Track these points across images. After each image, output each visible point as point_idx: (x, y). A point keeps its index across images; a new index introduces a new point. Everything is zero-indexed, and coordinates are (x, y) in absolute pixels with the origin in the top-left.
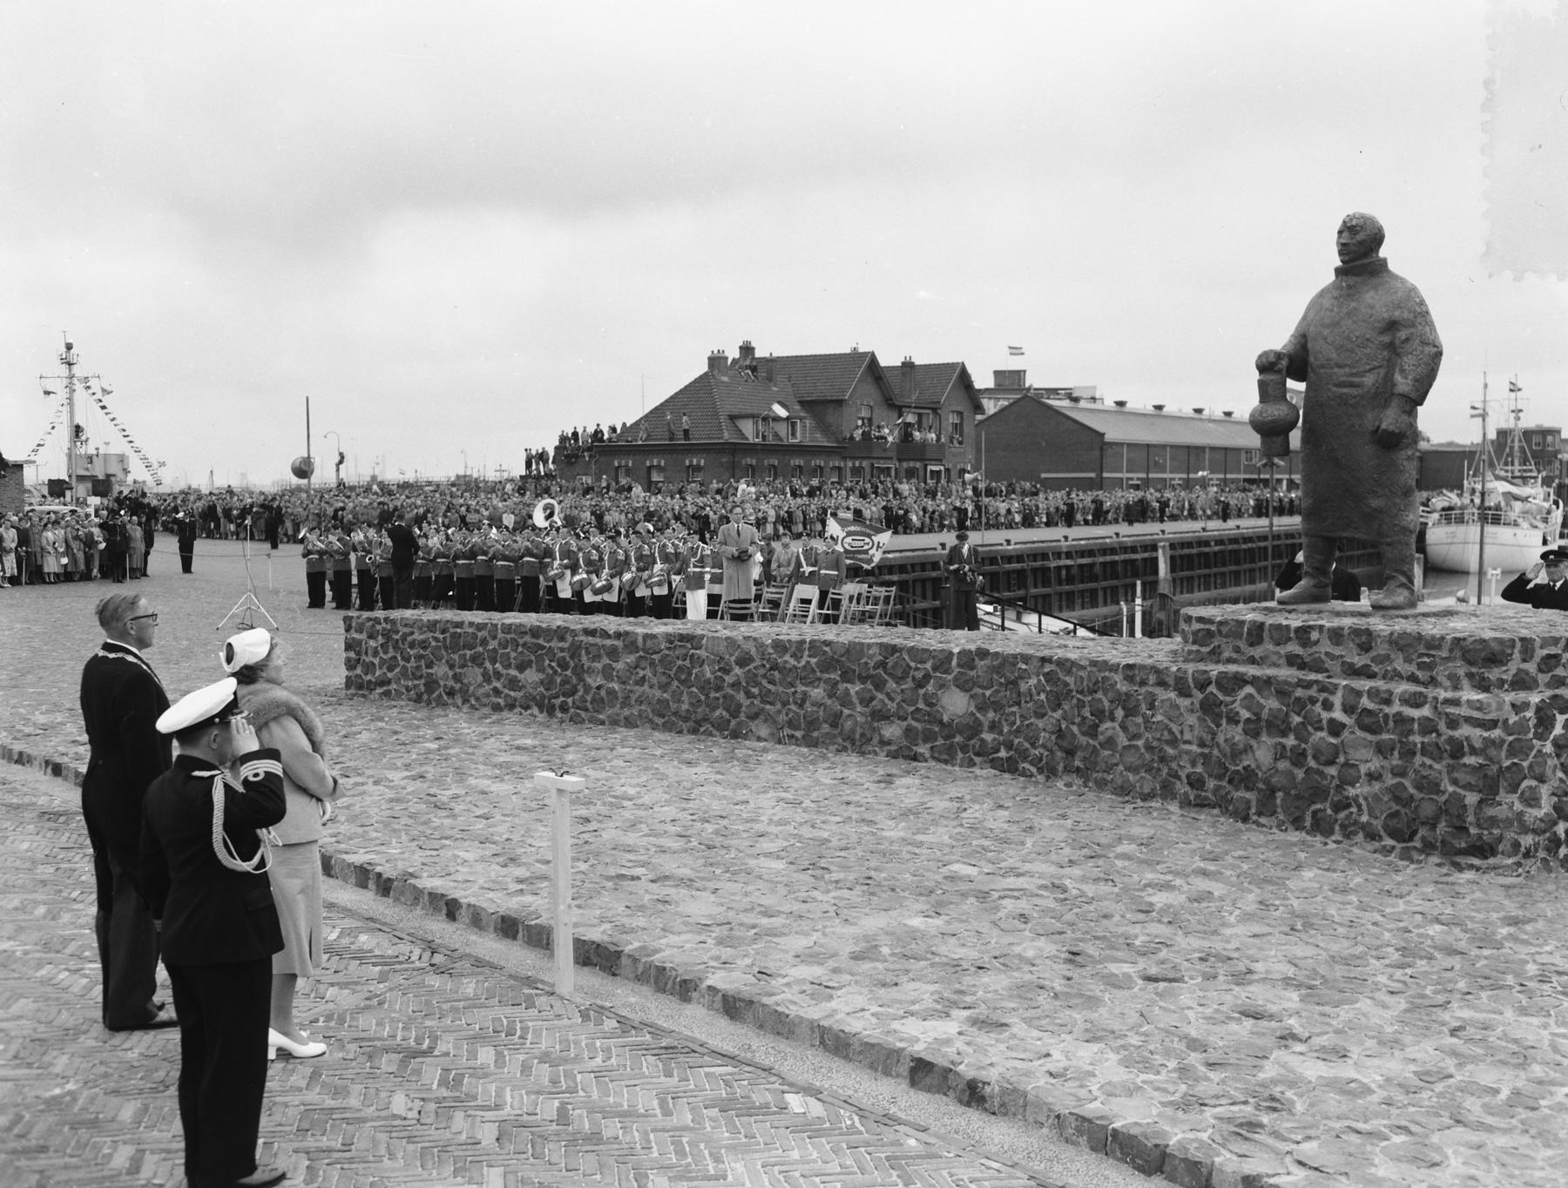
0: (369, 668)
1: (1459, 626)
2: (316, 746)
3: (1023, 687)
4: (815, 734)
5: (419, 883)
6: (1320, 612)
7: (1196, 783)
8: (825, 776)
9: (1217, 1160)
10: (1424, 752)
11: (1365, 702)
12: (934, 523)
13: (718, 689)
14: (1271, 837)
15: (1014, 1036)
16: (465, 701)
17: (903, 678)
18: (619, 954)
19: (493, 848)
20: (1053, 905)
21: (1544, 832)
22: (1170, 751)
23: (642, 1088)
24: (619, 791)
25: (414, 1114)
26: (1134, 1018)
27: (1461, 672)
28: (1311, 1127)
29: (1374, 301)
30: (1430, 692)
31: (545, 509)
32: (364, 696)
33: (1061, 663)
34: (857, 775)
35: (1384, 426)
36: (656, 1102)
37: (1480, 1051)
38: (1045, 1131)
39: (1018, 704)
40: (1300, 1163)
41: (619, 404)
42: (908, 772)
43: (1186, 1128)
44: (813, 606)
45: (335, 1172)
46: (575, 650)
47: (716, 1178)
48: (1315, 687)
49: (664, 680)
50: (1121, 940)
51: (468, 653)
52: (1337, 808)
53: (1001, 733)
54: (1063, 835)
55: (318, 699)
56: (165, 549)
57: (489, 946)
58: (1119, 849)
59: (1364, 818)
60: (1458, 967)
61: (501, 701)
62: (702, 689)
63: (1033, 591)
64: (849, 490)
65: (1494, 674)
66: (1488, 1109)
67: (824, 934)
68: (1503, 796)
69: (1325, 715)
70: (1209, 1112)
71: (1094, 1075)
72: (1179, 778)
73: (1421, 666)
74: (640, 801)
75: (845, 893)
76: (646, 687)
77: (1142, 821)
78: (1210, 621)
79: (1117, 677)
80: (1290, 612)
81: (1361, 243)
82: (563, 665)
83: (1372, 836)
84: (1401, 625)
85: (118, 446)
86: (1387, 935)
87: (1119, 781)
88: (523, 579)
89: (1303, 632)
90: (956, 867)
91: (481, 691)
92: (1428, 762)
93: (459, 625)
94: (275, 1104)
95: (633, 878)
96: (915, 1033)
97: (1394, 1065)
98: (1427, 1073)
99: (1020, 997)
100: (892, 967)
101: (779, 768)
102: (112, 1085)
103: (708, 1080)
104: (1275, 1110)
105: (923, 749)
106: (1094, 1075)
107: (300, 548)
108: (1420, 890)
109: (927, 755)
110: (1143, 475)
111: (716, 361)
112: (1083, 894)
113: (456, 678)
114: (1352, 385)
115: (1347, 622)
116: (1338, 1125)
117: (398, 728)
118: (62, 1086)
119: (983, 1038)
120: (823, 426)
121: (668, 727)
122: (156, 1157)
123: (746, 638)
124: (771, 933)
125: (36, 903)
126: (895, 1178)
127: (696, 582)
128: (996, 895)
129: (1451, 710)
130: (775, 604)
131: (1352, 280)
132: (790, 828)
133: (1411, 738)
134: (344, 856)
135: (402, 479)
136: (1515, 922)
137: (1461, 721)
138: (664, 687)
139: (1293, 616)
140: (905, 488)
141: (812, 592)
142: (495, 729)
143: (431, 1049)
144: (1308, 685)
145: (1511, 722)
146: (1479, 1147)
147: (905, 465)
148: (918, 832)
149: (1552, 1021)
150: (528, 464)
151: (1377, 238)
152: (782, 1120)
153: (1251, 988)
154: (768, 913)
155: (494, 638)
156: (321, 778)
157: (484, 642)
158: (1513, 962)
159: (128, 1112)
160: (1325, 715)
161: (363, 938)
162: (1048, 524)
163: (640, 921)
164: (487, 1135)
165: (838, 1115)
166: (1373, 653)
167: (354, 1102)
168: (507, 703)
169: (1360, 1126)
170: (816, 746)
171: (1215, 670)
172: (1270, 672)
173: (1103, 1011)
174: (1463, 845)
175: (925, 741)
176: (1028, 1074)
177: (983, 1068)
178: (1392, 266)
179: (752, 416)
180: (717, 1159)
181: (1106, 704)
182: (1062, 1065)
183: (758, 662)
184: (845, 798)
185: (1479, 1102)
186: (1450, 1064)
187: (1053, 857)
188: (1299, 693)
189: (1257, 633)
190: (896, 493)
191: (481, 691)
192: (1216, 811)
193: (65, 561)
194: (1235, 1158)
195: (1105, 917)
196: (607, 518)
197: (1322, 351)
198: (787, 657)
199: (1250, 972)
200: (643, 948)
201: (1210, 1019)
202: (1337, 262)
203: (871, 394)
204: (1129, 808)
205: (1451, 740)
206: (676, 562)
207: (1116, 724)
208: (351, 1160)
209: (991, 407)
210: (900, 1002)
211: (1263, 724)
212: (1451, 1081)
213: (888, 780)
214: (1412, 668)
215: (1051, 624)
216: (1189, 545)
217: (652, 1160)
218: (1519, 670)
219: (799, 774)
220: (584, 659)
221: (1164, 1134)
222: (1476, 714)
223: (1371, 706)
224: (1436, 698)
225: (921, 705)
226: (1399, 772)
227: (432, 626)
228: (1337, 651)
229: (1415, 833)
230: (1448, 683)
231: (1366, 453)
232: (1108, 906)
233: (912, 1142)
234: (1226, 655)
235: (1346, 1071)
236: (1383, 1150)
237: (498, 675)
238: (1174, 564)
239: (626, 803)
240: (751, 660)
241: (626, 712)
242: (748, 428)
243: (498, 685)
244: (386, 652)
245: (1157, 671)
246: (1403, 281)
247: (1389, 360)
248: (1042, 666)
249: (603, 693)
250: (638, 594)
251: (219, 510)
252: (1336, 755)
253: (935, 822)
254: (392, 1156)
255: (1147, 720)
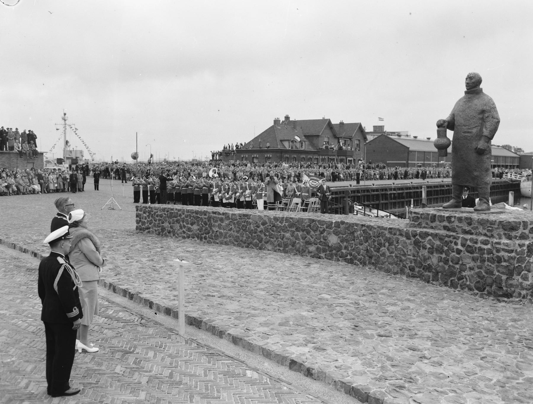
0: (144, 223)
1: (503, 217)
2: (97, 249)
3: (356, 234)
4: (287, 249)
5: (142, 296)
6: (457, 211)
7: (412, 269)
8: (287, 263)
9: (385, 398)
10: (488, 260)
11: (469, 243)
12: (349, 177)
13: (255, 233)
14: (436, 289)
15: (327, 354)
16: (174, 235)
17: (316, 231)
18: (201, 321)
19: (169, 285)
20: (353, 309)
21: (530, 289)
22: (403, 258)
23: (199, 366)
24: (216, 266)
25: (122, 373)
26: (370, 349)
27: (502, 233)
28: (421, 389)
29: (477, 103)
30: (491, 240)
31: (213, 171)
32: (142, 233)
33: (368, 227)
34: (298, 262)
35: (479, 147)
36: (203, 372)
37: (489, 365)
38: (331, 386)
39: (354, 240)
40: (414, 401)
41: (244, 135)
42: (316, 263)
43: (377, 387)
44: (299, 206)
45: (91, 391)
46: (209, 219)
47: (216, 398)
48: (452, 237)
49: (238, 229)
50: (374, 322)
51: (175, 219)
52: (459, 279)
53: (348, 250)
54: (363, 285)
55: (127, 233)
56: (90, 181)
57: (161, 318)
58: (381, 291)
59: (468, 283)
60: (490, 336)
61: (185, 235)
62: (250, 233)
63: (382, 202)
64: (320, 166)
65: (513, 234)
66: (486, 386)
67: (272, 317)
68: (515, 277)
69: (455, 247)
70: (388, 382)
71: (351, 368)
72: (406, 267)
73: (488, 231)
74: (222, 270)
75: (283, 303)
76: (232, 232)
77: (392, 282)
78: (418, 214)
79: (386, 232)
80: (446, 211)
81: (473, 83)
82: (206, 224)
83: (470, 289)
84: (484, 217)
85: (80, 147)
86: (468, 324)
87: (386, 268)
88: (203, 194)
89: (449, 218)
90: (323, 295)
91: (179, 232)
92: (490, 264)
93: (172, 209)
94: (78, 367)
95: (213, 296)
96: (293, 351)
97: (458, 369)
98: (468, 372)
99: (333, 340)
100: (292, 328)
101: (272, 260)
102: (27, 359)
103: (221, 365)
104: (411, 382)
105: (322, 255)
106: (351, 368)
107: (132, 183)
108: (484, 309)
109: (324, 257)
110: (423, 162)
111: (276, 122)
112: (365, 306)
113: (171, 227)
114: (468, 132)
115: (464, 215)
116: (431, 389)
117: (149, 244)
118: (11, 359)
119: (316, 354)
120: (312, 144)
121: (239, 245)
122: (34, 384)
123: (265, 216)
124: (254, 316)
125: (18, 298)
126: (276, 400)
127: (260, 197)
128: (335, 305)
129: (497, 246)
130: (286, 204)
131: (470, 96)
132: (270, 281)
133: (484, 256)
134: (120, 286)
135: (174, 160)
136: (515, 320)
137: (501, 250)
138: (238, 232)
139: (447, 212)
140: (339, 165)
141: (299, 201)
142: (182, 245)
143: (133, 351)
144: (450, 236)
145: (518, 251)
146: (479, 399)
147: (340, 157)
148: (314, 283)
149: (518, 357)
150: (213, 156)
151: (479, 81)
152: (244, 379)
153: (414, 340)
154: (255, 309)
155: (184, 214)
156: (98, 260)
157: (180, 215)
158: (510, 335)
159: (29, 368)
160: (455, 247)
161: (121, 313)
162: (388, 179)
163: (211, 311)
164: (144, 380)
165: (262, 378)
166: (472, 226)
167: (103, 368)
168: (188, 236)
169: (440, 389)
170: (287, 253)
171: (418, 230)
172: (437, 232)
173: (361, 346)
174: (501, 293)
175: (323, 252)
176: (328, 366)
177: (313, 364)
178: (484, 91)
179: (288, 140)
180: (218, 392)
181: (383, 241)
182: (340, 364)
183: (268, 224)
184: (292, 271)
185: (484, 383)
186: (478, 370)
187: (358, 293)
188: (447, 239)
189: (433, 218)
190: (336, 167)
191: (179, 232)
192: (419, 279)
193: (56, 185)
194: (392, 398)
195: (370, 314)
196: (237, 174)
197: (459, 120)
198: (278, 223)
199: (416, 334)
200: (209, 320)
201: (397, 351)
202: (465, 89)
203: (329, 133)
204: (389, 277)
205: (498, 257)
206: (254, 190)
207: (386, 248)
208: (97, 387)
209: (370, 138)
210: (291, 340)
211: (434, 249)
212: (476, 375)
213: (308, 265)
214: (485, 231)
215: (382, 213)
216: (437, 187)
217: (198, 391)
218: (522, 232)
219: (279, 262)
220: (212, 221)
221: (369, 389)
222: (506, 248)
223: (470, 244)
224: (492, 242)
225: (322, 240)
226: (480, 267)
227: (164, 210)
228: (460, 225)
229: (485, 289)
230: (497, 237)
231: (473, 156)
232: (372, 310)
233: (285, 388)
234: (423, 225)
235: (440, 370)
236: (445, 398)
237: (184, 227)
238: (429, 193)
239: (218, 271)
240: (266, 223)
241: (225, 240)
242: (286, 144)
243: (184, 230)
244: (149, 218)
245: (400, 230)
246: (488, 96)
247: (482, 124)
248: (362, 228)
249: (218, 233)
250: (241, 200)
251: (110, 169)
252: (459, 261)
253: (320, 280)
254: (111, 386)
255: (396, 247)
